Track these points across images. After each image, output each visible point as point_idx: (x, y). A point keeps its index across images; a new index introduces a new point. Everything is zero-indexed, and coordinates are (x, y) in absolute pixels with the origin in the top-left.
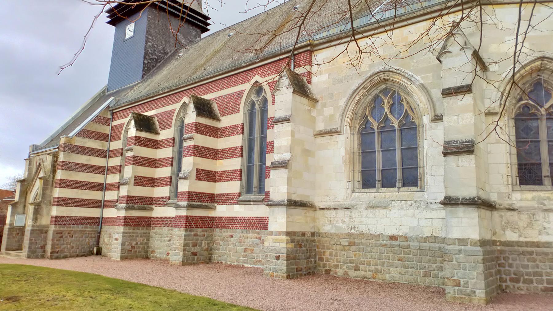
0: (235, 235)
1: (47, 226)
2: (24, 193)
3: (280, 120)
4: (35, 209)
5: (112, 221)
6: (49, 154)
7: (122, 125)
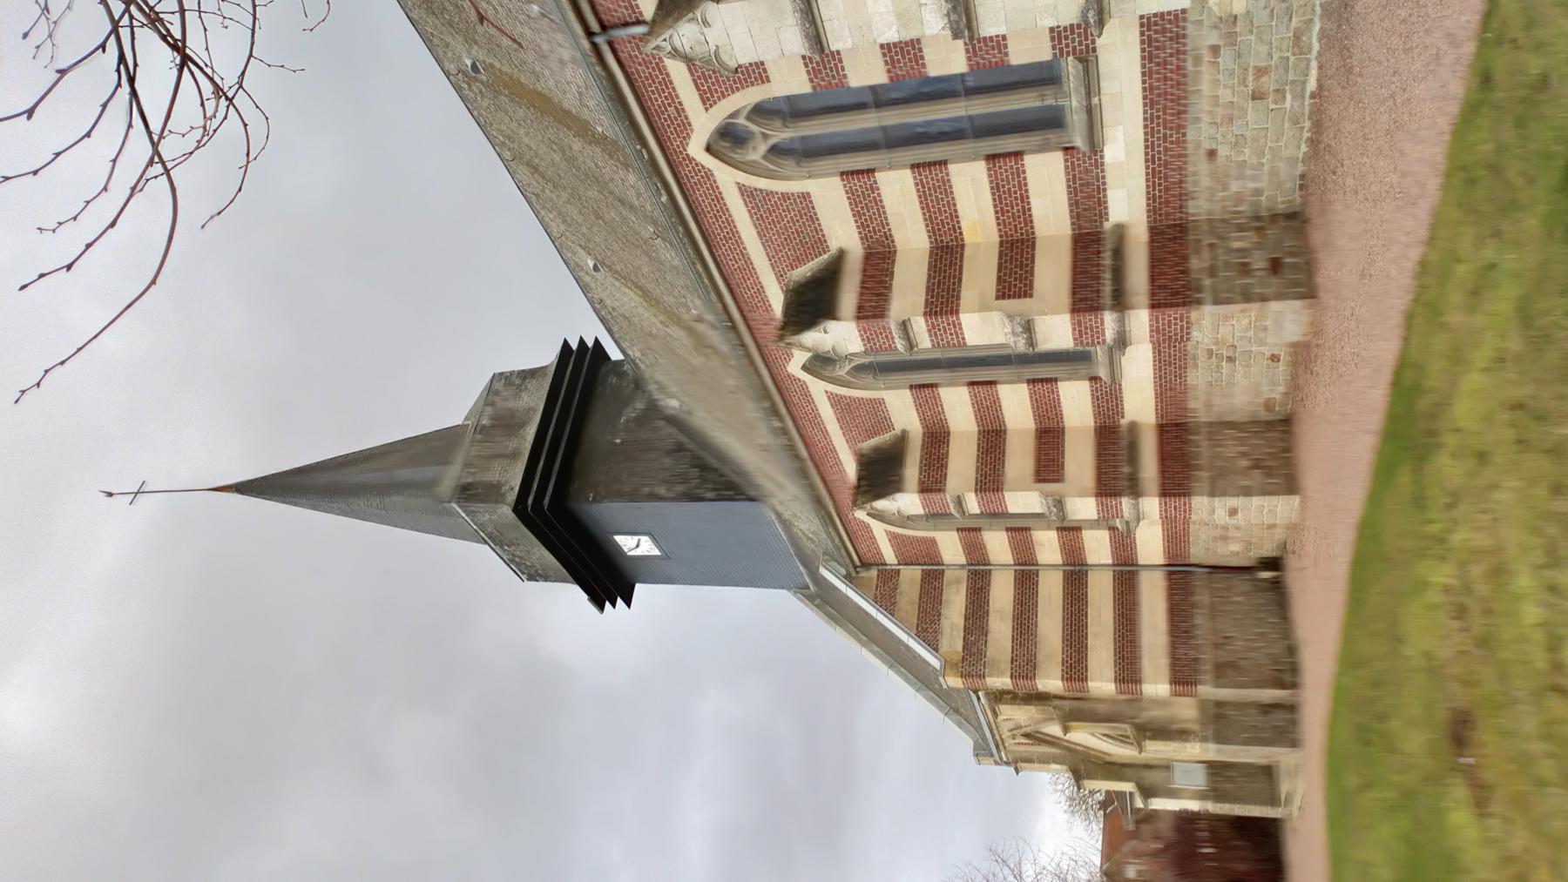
0: (1207, 145)
1: (1203, 705)
2: (1113, 769)
3: (812, 30)
4: (1153, 738)
5: (1176, 536)
6: (995, 714)
7: (893, 538)
